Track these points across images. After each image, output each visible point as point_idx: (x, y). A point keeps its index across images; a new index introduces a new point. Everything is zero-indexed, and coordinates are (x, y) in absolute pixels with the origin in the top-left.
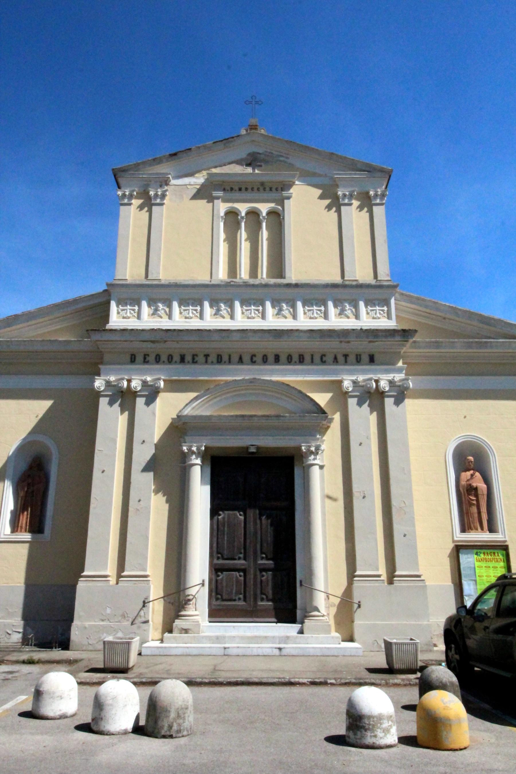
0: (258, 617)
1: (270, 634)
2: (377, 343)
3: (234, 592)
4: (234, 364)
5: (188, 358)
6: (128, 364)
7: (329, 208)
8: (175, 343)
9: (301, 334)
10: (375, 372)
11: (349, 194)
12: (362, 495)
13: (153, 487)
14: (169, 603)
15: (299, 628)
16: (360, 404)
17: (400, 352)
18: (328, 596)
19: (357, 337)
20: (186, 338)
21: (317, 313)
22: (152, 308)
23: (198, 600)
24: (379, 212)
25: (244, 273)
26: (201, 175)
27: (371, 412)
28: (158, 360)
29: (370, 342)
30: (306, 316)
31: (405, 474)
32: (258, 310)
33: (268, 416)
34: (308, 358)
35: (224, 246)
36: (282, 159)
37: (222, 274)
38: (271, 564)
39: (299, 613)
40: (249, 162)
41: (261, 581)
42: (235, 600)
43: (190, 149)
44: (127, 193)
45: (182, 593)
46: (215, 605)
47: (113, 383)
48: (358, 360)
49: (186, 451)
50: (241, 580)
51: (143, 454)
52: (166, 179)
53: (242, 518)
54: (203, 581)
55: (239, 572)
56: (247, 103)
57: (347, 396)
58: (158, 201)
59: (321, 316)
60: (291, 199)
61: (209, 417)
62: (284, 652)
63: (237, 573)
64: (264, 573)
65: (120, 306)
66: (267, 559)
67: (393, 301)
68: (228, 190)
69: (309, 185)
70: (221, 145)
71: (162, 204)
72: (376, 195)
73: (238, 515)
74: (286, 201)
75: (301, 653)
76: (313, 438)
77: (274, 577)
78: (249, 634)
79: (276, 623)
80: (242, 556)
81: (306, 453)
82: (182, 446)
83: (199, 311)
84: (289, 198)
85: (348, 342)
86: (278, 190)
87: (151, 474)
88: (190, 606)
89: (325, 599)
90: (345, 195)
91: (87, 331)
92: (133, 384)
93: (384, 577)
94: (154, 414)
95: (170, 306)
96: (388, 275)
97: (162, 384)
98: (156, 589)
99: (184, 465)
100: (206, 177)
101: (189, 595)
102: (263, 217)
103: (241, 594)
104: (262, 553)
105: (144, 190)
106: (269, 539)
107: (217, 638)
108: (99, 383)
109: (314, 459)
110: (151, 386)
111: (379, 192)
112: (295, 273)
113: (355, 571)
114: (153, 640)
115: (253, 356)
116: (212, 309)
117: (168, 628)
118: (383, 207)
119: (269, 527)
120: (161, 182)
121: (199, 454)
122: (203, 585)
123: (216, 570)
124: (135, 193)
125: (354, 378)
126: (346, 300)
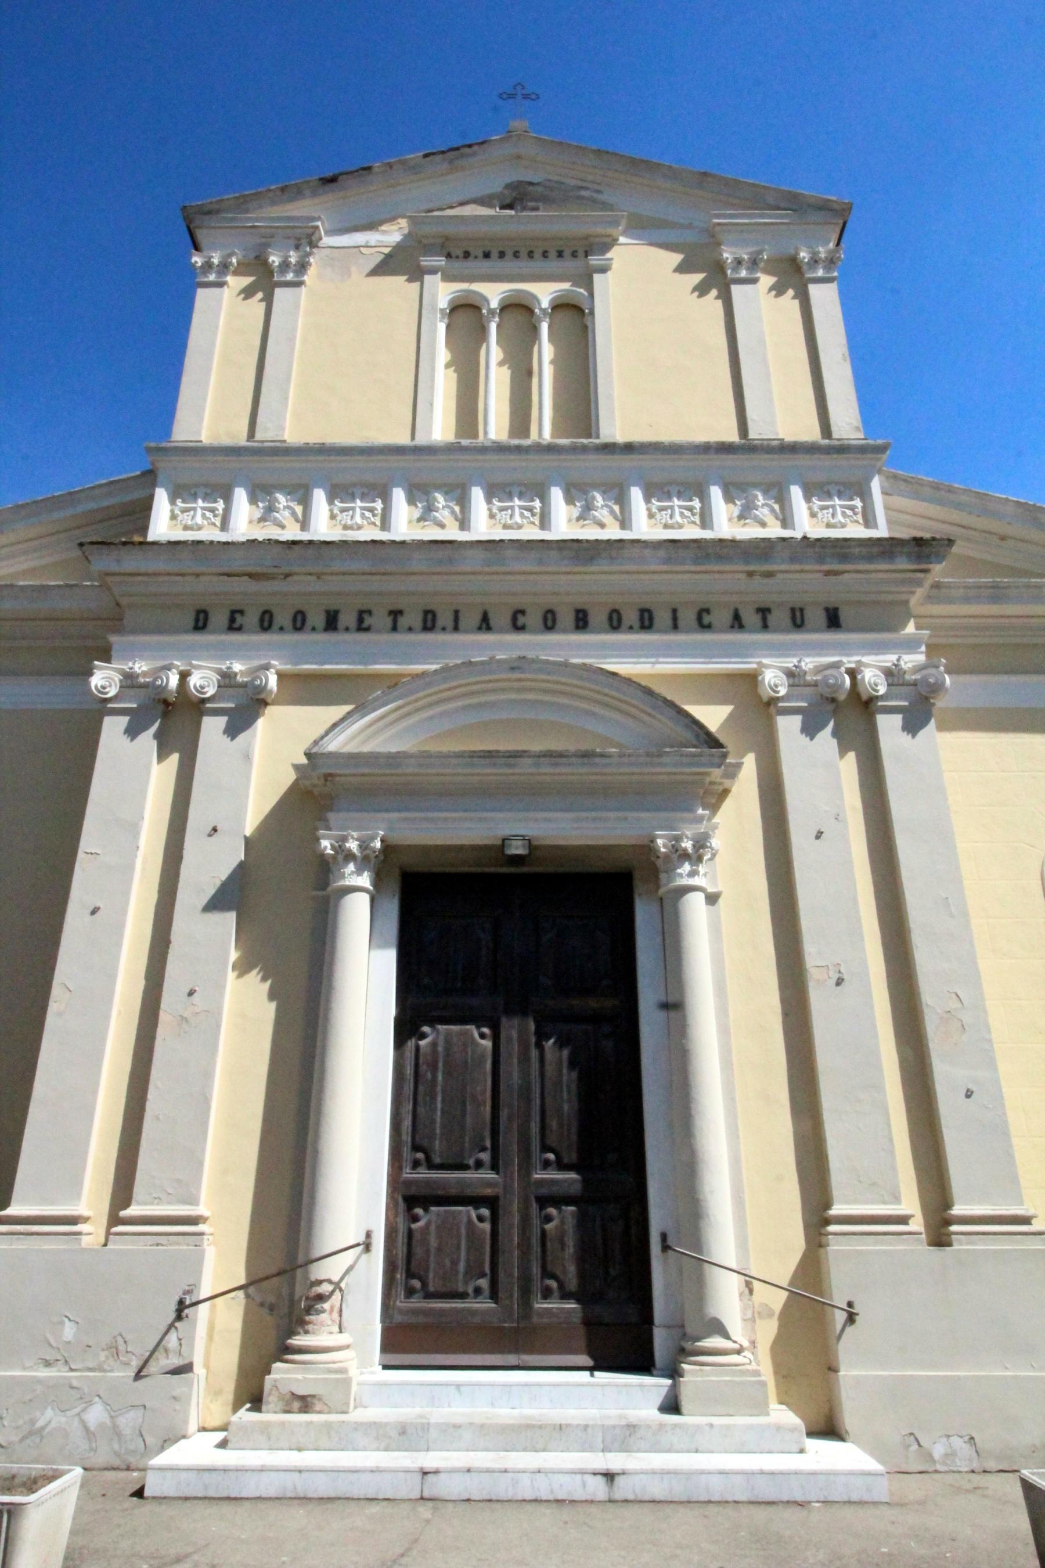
0: (531, 1351)
1: (572, 1414)
2: (846, 576)
3: (462, 1266)
4: (466, 632)
5: (348, 618)
6: (186, 632)
7: (701, 290)
8: (314, 578)
9: (647, 552)
10: (845, 648)
11: (749, 259)
12: (836, 976)
13: (234, 955)
14: (262, 1305)
15: (664, 1391)
16: (810, 729)
17: (907, 602)
18: (748, 1284)
19: (793, 560)
20: (337, 566)
21: (682, 514)
22: (261, 505)
23: (348, 1298)
24: (825, 298)
25: (496, 426)
26: (395, 227)
27: (843, 752)
28: (266, 622)
29: (828, 573)
30: (653, 521)
31: (952, 916)
32: (531, 510)
33: (561, 755)
34: (663, 617)
35: (445, 375)
36: (583, 193)
37: (440, 427)
38: (574, 1181)
39: (661, 1340)
40: (508, 201)
41: (544, 1233)
42: (463, 1296)
43: (369, 169)
44: (216, 261)
45: (299, 1272)
46: (401, 1311)
47: (142, 680)
48: (798, 621)
49: (329, 851)
50: (483, 1231)
51: (210, 863)
52: (310, 231)
53: (487, 1044)
54: (368, 1235)
55: (476, 1208)
56: (504, 96)
57: (772, 710)
58: (290, 276)
59: (694, 523)
60: (609, 273)
61: (394, 759)
62: (624, 1488)
63: (470, 1208)
64: (552, 1211)
65: (179, 502)
66: (561, 1166)
67: (876, 485)
68: (457, 257)
69: (651, 244)
70: (439, 164)
71: (299, 284)
72: (815, 261)
73: (476, 1035)
74: (597, 278)
75: (679, 1490)
76: (686, 815)
77: (582, 1221)
78: (506, 1413)
79: (592, 1369)
80: (486, 1156)
81: (667, 857)
82: (317, 840)
83: (380, 511)
84: (604, 270)
85: (770, 575)
86: (581, 255)
87: (231, 917)
88: (323, 1316)
89: (741, 1294)
90: (739, 262)
91: (81, 545)
92: (194, 681)
93: (917, 1224)
94: (247, 757)
95: (306, 501)
96: (857, 429)
97: (272, 681)
98: (222, 1261)
99: (320, 893)
100: (406, 231)
101: (320, 1282)
102: (541, 309)
103: (483, 1275)
104: (545, 1148)
105: (257, 257)
106: (566, 1107)
107: (403, 1430)
108: (104, 679)
109: (693, 874)
110: (244, 685)
111: (822, 252)
112: (619, 421)
113: (828, 1206)
114: (204, 1429)
115: (519, 612)
116: (413, 508)
117: (251, 1394)
118: (834, 286)
119: (565, 1071)
120: (299, 239)
121: (364, 862)
122: (367, 1247)
123: (408, 1199)
124: (234, 260)
125: (790, 663)
126: (755, 485)
